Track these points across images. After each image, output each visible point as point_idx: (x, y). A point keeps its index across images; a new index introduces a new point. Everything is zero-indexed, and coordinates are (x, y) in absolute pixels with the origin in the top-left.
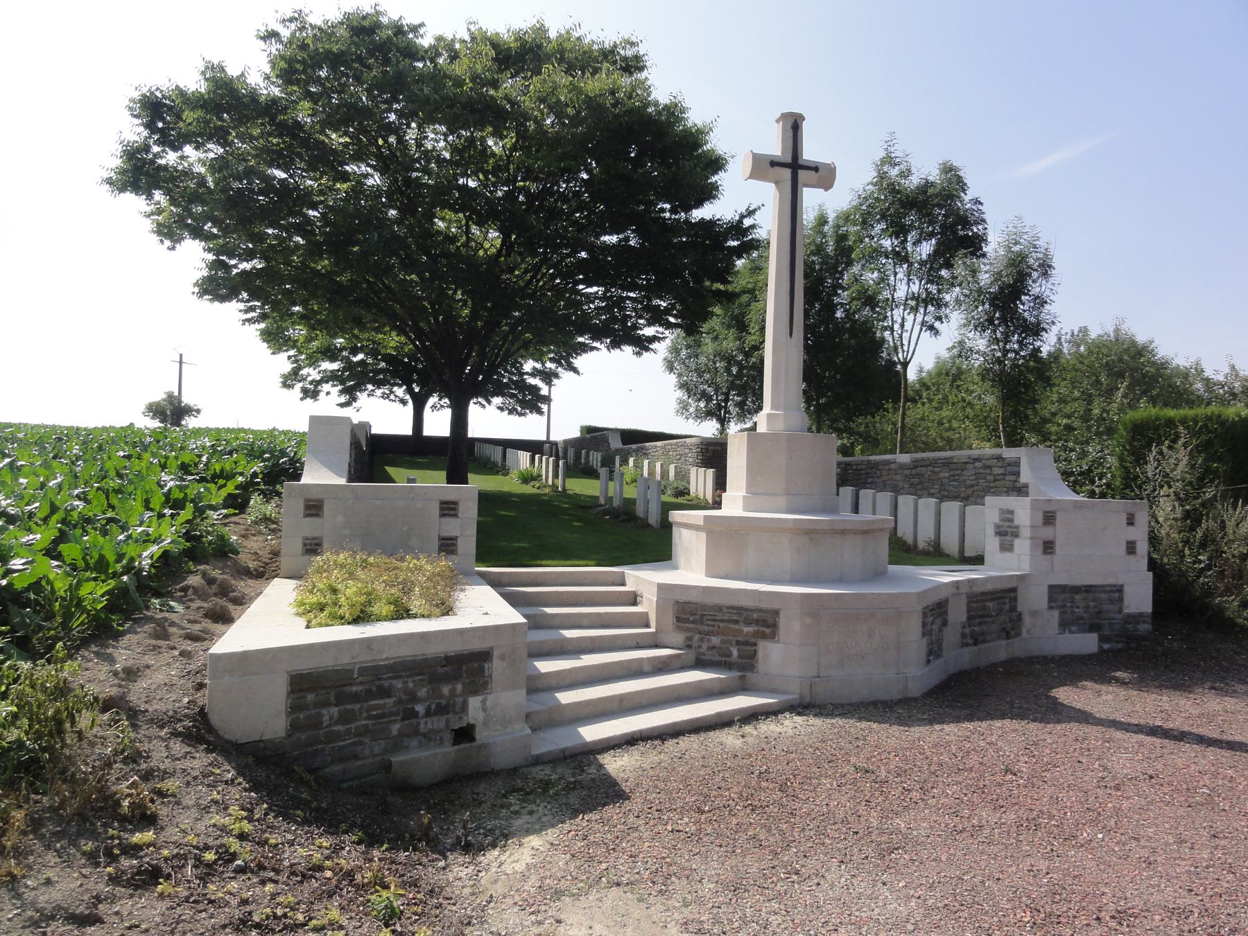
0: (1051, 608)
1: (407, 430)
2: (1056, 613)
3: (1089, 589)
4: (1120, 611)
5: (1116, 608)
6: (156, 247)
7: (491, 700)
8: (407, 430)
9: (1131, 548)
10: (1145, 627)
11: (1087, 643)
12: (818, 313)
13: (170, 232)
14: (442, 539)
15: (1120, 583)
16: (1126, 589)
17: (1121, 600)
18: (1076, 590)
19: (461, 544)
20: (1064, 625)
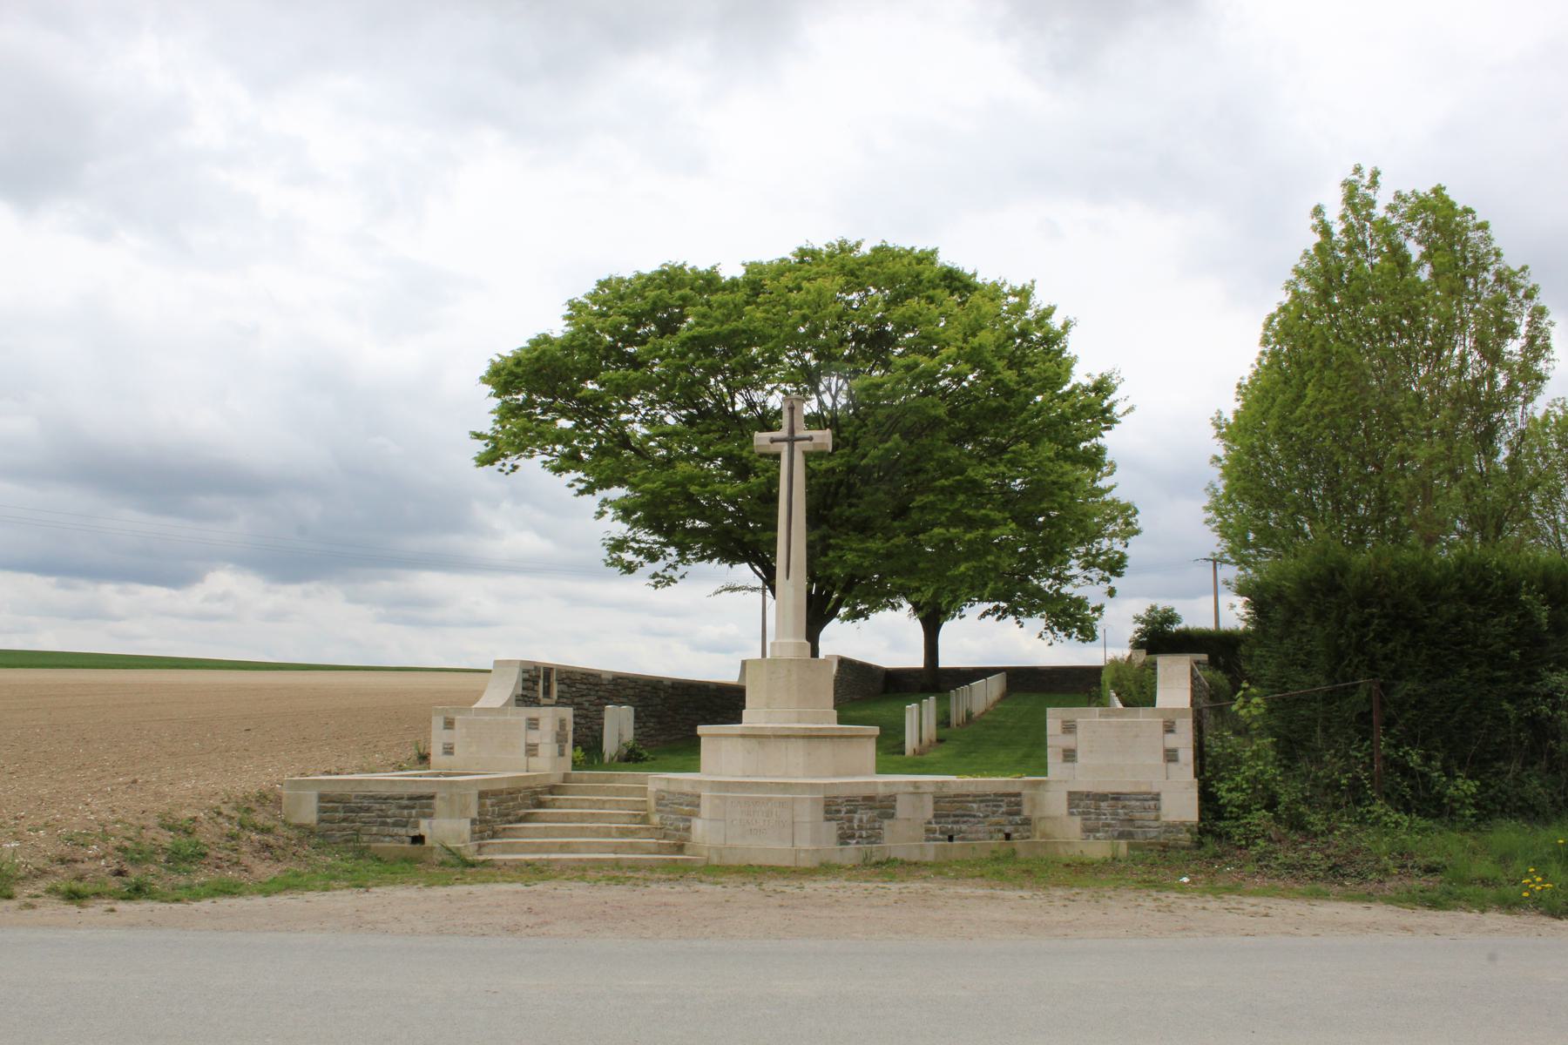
0: (1072, 814)
1: (916, 660)
2: (1078, 819)
3: (1117, 797)
4: (1157, 819)
5: (1152, 815)
6: (1282, 284)
7: (435, 822)
8: (916, 660)
9: (1171, 756)
10: (1185, 838)
11: (1098, 849)
12: (1508, 331)
13: (1314, 229)
14: (528, 745)
15: (1155, 790)
16: (1163, 796)
17: (1157, 808)
18: (1103, 797)
19: (541, 749)
20: (1089, 831)
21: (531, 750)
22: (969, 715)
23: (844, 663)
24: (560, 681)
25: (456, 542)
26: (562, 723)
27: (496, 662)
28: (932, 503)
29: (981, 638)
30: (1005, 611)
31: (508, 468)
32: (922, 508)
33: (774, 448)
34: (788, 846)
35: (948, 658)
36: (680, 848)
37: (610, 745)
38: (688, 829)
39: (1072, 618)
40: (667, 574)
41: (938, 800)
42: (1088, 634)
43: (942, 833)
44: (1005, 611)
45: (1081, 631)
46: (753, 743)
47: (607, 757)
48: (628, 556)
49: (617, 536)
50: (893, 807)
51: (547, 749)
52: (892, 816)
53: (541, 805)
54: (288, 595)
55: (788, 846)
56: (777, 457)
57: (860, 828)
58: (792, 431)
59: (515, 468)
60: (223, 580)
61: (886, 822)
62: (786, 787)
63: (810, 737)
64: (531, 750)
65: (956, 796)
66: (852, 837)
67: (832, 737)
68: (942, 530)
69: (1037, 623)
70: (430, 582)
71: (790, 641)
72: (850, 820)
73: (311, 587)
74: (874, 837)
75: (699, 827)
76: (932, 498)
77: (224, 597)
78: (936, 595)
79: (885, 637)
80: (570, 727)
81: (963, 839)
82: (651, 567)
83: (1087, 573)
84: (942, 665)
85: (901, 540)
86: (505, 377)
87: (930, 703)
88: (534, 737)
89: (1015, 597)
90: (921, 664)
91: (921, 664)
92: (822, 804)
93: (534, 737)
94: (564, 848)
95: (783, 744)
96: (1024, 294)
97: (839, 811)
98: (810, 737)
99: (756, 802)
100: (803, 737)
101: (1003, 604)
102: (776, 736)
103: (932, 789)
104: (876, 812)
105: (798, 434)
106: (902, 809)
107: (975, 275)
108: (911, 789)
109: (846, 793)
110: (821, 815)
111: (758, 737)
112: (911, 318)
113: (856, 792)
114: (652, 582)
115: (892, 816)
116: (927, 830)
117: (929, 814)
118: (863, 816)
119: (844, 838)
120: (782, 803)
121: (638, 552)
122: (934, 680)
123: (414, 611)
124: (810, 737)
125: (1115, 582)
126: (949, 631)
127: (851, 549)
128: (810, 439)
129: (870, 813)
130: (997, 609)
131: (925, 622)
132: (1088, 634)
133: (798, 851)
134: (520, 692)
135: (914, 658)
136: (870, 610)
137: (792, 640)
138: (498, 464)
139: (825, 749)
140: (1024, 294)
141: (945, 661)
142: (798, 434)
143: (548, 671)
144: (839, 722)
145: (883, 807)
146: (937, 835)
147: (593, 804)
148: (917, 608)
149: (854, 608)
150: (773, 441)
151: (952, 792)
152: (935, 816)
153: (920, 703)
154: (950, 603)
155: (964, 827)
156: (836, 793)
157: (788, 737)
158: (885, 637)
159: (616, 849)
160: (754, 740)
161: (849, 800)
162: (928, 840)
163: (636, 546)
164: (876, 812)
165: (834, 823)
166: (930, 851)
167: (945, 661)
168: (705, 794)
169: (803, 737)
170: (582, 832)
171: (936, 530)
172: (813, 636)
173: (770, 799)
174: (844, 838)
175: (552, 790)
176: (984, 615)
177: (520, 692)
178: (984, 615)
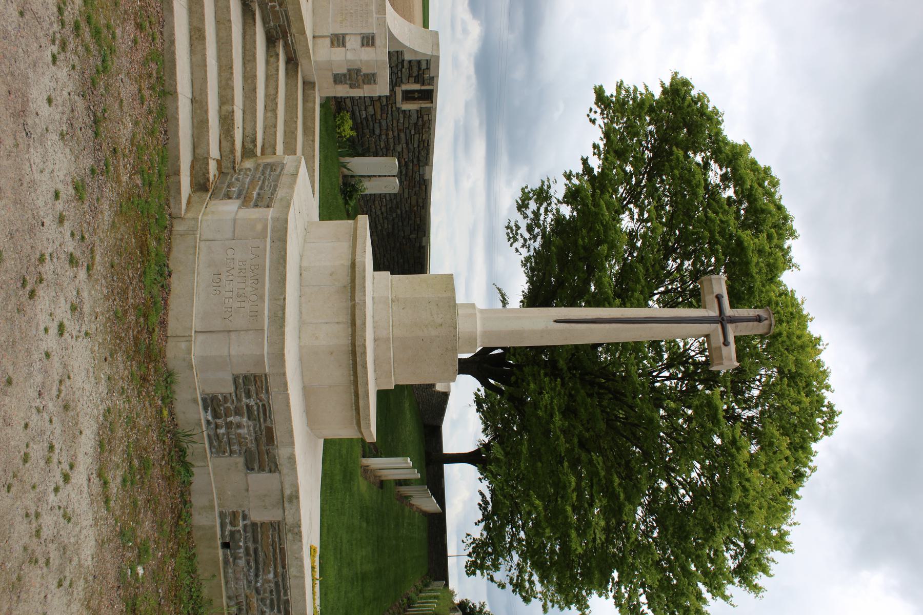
14: (344, 36)
21: (338, 40)
22: (407, 497)
23: (445, 396)
24: (420, 112)
25: (504, 159)
26: (370, 78)
27: (436, 33)
28: (597, 474)
29: (465, 494)
30: (485, 509)
31: (593, 116)
32: (591, 461)
33: (710, 299)
34: (196, 324)
35: (450, 470)
36: (201, 186)
37: (359, 165)
38: (228, 196)
39: (484, 556)
40: (519, 237)
41: (276, 527)
42: (471, 569)
43: (232, 534)
44: (485, 509)
45: (474, 563)
46: (345, 279)
47: (347, 159)
48: (533, 205)
49: (552, 191)
50: (261, 469)
51: (341, 58)
52: (249, 467)
53: (271, 41)
54: (468, 67)
55: (196, 324)
56: (699, 304)
57: (229, 425)
58: (733, 320)
59: (593, 121)
60: (475, 29)
61: (241, 460)
62: (279, 320)
63: (354, 353)
64: (338, 40)
65: (282, 550)
66: (216, 415)
67: (355, 383)
68: (573, 484)
69: (478, 532)
70: (479, 148)
71: (477, 334)
72: (238, 412)
73: (474, 80)
74: (219, 446)
75: (229, 208)
76: (603, 473)
77: (465, 31)
78: (497, 460)
79: (463, 425)
80: (365, 91)
81: (226, 562)
82: (523, 224)
83: (514, 567)
84: (447, 467)
85: (563, 445)
86: (677, 91)
87: (416, 475)
88: (353, 43)
89: (497, 513)
90: (445, 451)
91: (445, 451)
92: (257, 371)
93: (353, 43)
94: (197, 35)
95: (344, 317)
96: (780, 543)
97: (248, 396)
98: (354, 353)
99: (258, 280)
100: (353, 345)
101: (490, 508)
102: (353, 308)
103: (289, 520)
104: (252, 446)
105: (730, 328)
106: (260, 481)
107: (797, 497)
108: (287, 492)
109: (276, 406)
110: (242, 371)
111: (352, 285)
112: (771, 444)
113: (278, 418)
114: (512, 224)
115: (249, 467)
116: (234, 514)
117: (257, 516)
118: (246, 428)
119: (211, 403)
120: (256, 315)
121: (536, 214)
122: (433, 461)
123: (463, 138)
124: (354, 354)
125: (510, 588)
126: (470, 471)
127: (552, 398)
128: (726, 343)
129: (250, 438)
130: (486, 503)
131: (477, 453)
132: (471, 569)
133: (188, 339)
134: (407, 57)
135: (450, 446)
136: (483, 413)
137: (479, 328)
138: (595, 108)
139: (338, 375)
140: (780, 543)
141: (448, 468)
142: (730, 328)
143: (429, 96)
144: (382, 395)
145: (263, 452)
146: (229, 528)
147: (271, 99)
148: (487, 446)
149: (485, 401)
150: (719, 298)
151: (289, 547)
152: (254, 525)
153: (414, 467)
154: (491, 472)
155: (242, 562)
156: (273, 390)
157: (353, 324)
158: (463, 425)
159: (198, 103)
160: (348, 279)
161: (265, 410)
162: (222, 515)
163: (542, 210)
164: (252, 446)
165: (232, 389)
166: (206, 520)
167: (448, 468)
168: (270, 213)
169: (353, 345)
170: (225, 68)
171: (573, 479)
172: (465, 367)
173: (262, 298)
174: (211, 403)
175: (292, 62)
176: (481, 494)
177: (407, 57)
178: (481, 494)
